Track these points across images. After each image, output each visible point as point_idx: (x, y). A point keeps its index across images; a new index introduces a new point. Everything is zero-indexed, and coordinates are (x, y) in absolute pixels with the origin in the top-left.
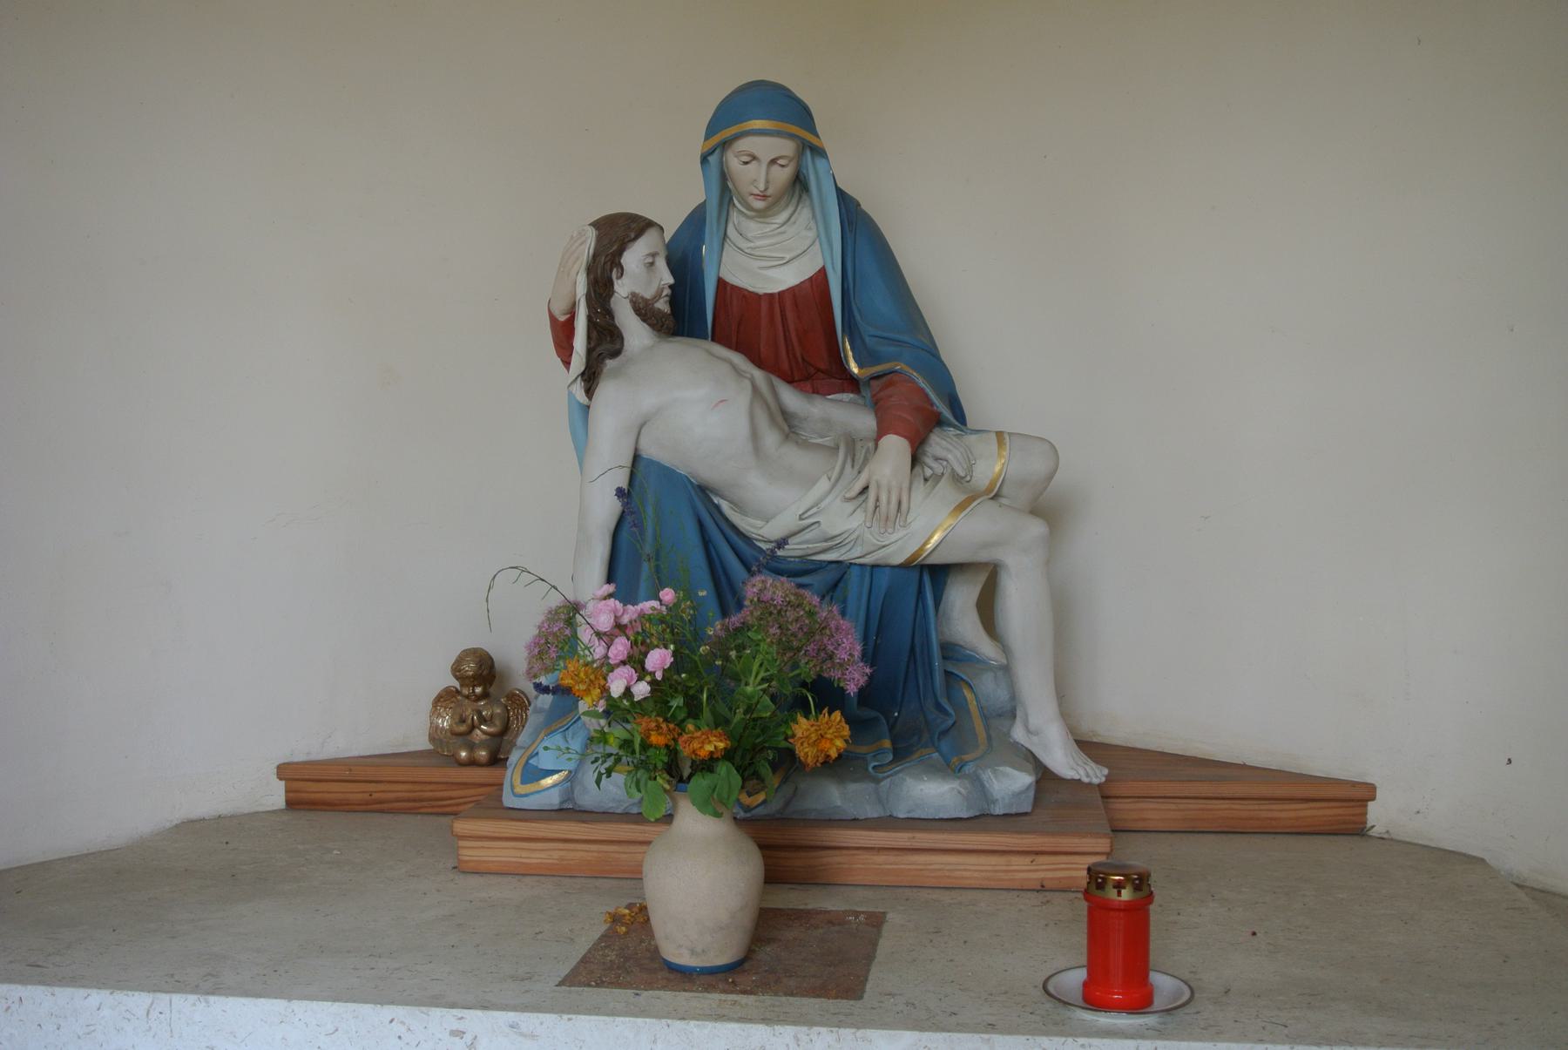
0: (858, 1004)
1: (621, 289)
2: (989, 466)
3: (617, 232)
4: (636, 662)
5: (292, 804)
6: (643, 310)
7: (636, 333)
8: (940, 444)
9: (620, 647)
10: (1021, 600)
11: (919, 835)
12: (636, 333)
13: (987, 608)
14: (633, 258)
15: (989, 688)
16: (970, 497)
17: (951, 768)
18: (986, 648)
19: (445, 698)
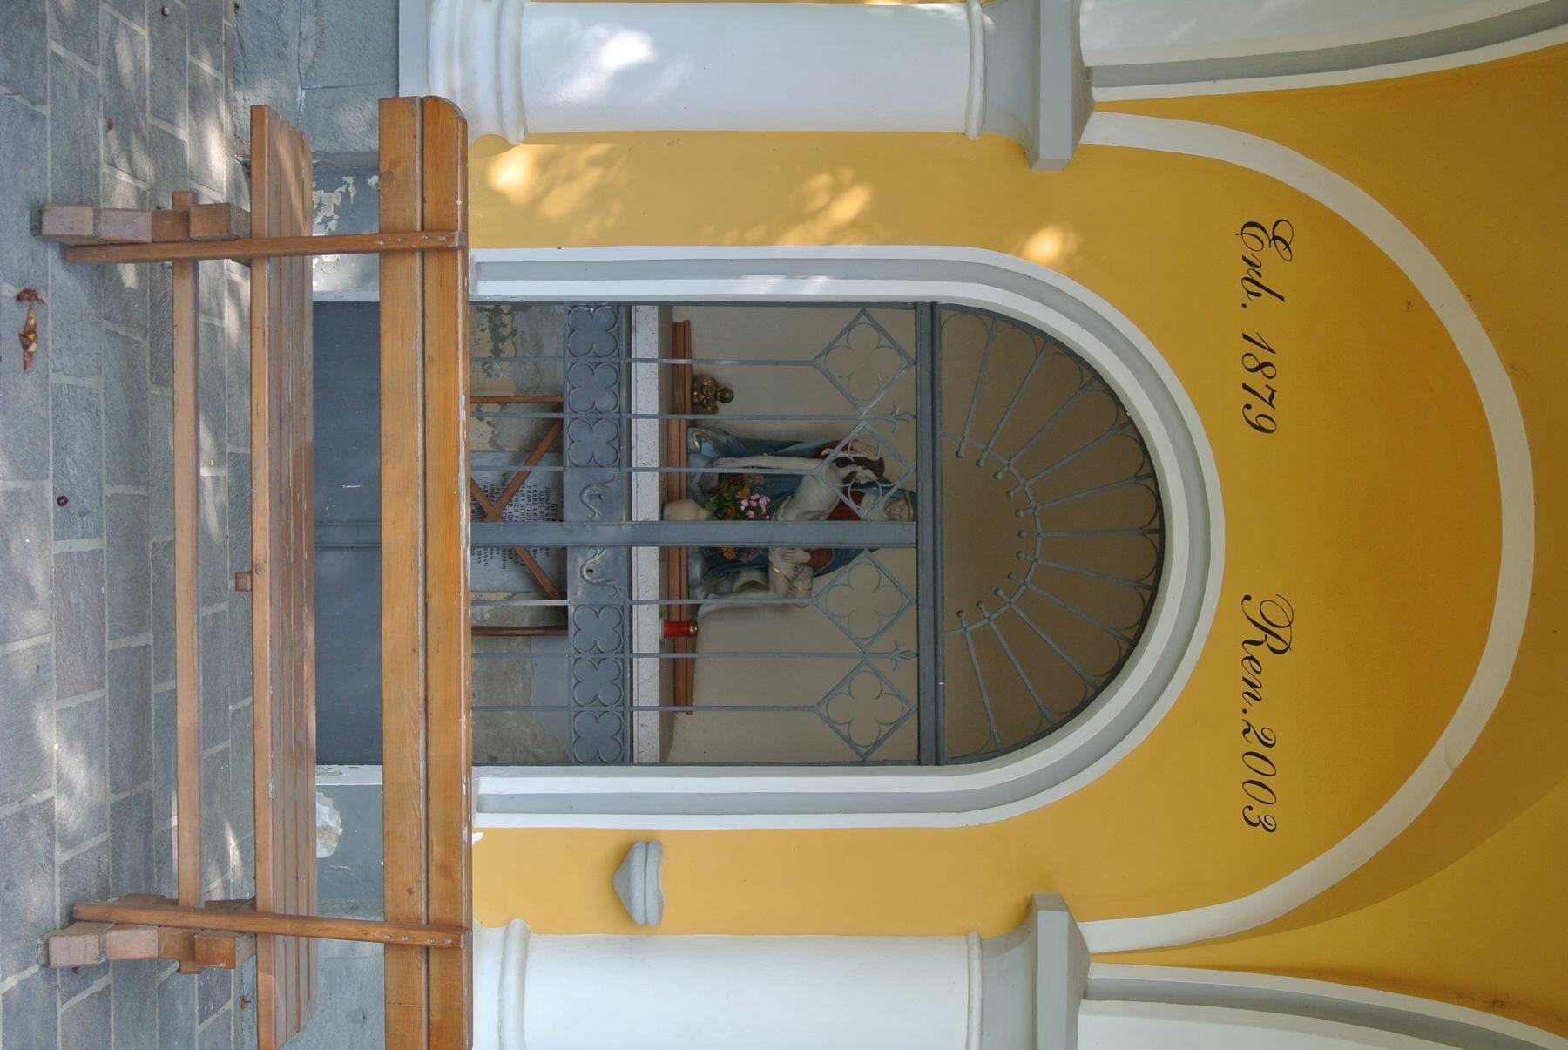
0: (28, 232)
1: (859, 469)
2: (800, 586)
3: (878, 467)
4: (749, 508)
5: (675, 325)
6: (852, 475)
7: (844, 472)
8: (808, 570)
9: (754, 504)
10: (754, 598)
11: (1463, 1020)
12: (844, 472)
13: (752, 585)
14: (868, 472)
15: (725, 586)
16: (790, 582)
17: (704, 575)
18: (738, 584)
19: (715, 382)
